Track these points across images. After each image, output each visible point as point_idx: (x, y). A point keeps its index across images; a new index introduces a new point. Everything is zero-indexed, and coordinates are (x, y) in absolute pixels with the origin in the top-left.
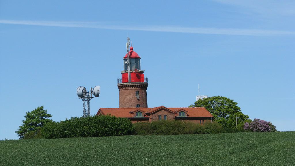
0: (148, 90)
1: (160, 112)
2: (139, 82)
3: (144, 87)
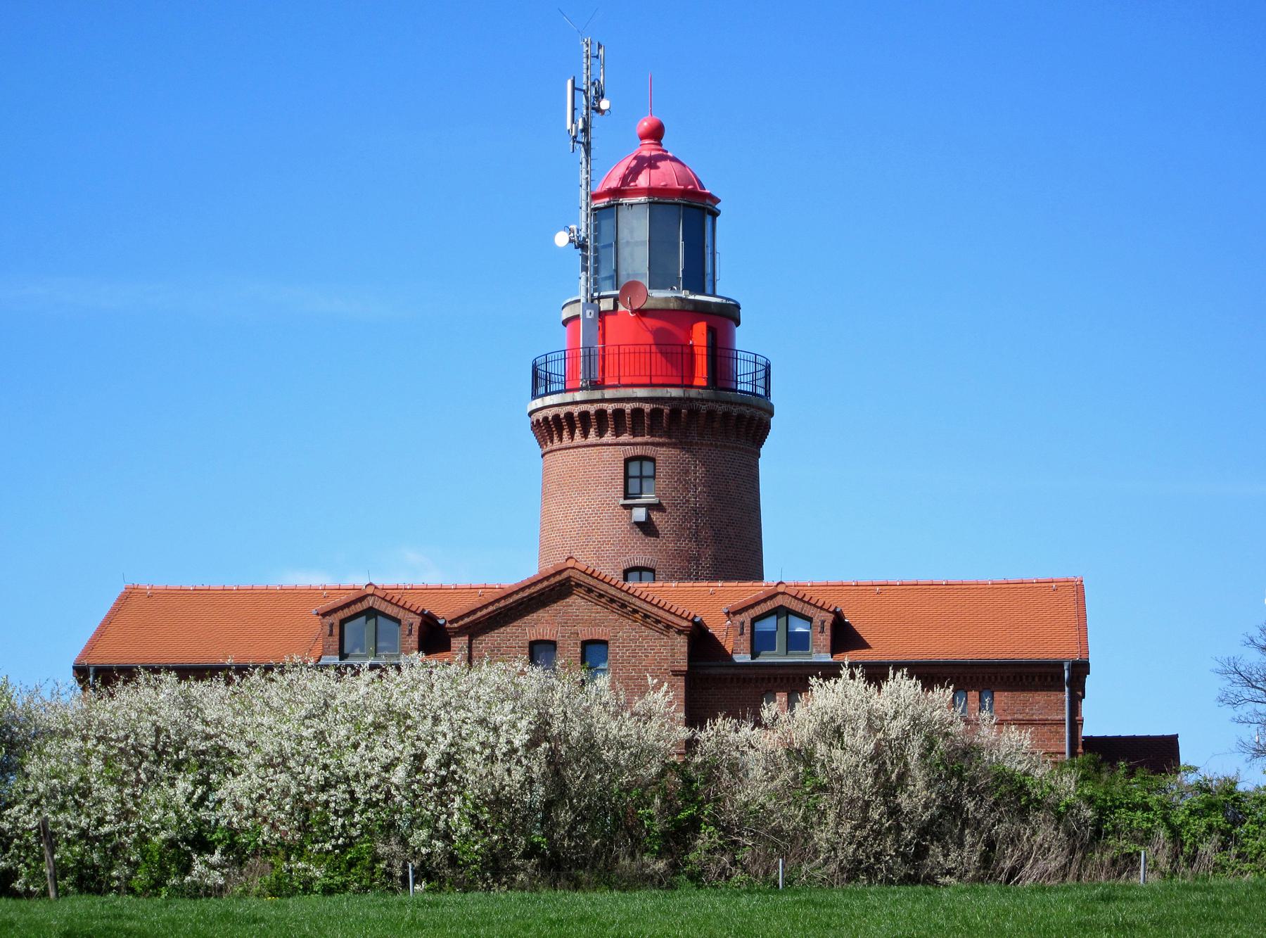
0: (773, 461)
1: (542, 614)
2: (651, 385)
3: (746, 424)
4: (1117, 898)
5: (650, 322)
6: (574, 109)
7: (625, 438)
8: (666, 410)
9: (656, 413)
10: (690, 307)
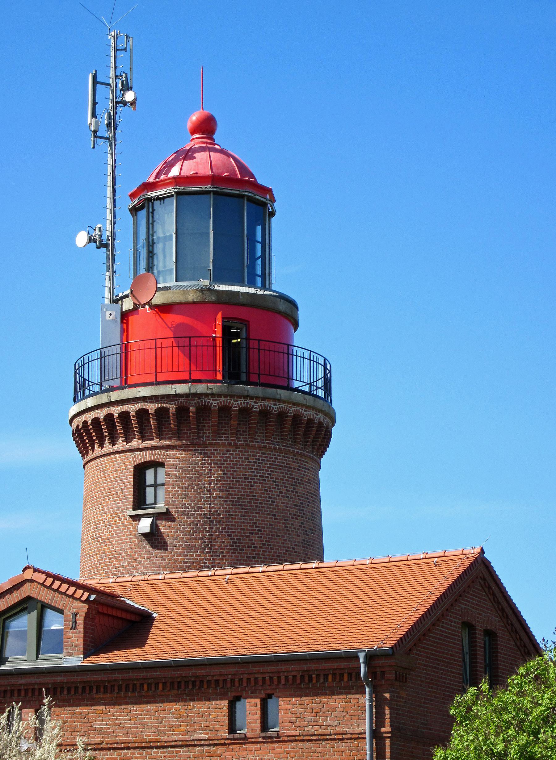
5: (174, 319)
6: (94, 103)
7: (135, 443)
8: (172, 409)
9: (161, 413)
10: (212, 298)
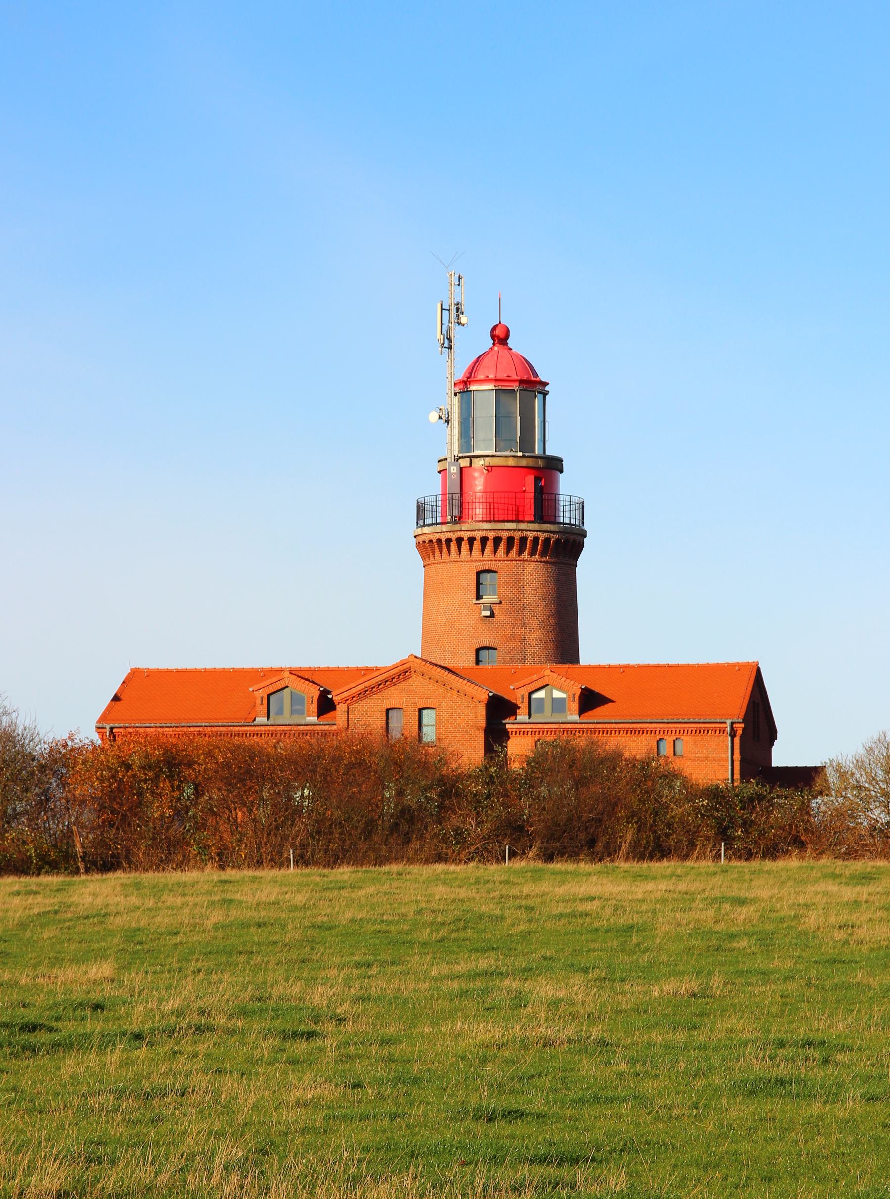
3: (566, 547)
4: (391, 833)
6: (442, 324)
